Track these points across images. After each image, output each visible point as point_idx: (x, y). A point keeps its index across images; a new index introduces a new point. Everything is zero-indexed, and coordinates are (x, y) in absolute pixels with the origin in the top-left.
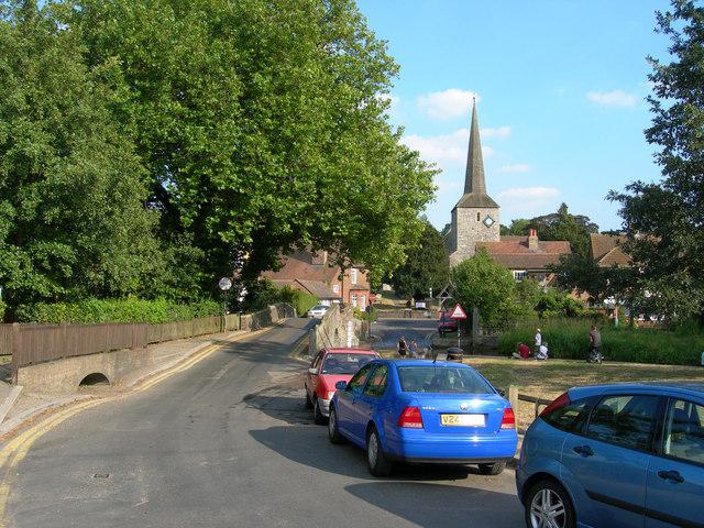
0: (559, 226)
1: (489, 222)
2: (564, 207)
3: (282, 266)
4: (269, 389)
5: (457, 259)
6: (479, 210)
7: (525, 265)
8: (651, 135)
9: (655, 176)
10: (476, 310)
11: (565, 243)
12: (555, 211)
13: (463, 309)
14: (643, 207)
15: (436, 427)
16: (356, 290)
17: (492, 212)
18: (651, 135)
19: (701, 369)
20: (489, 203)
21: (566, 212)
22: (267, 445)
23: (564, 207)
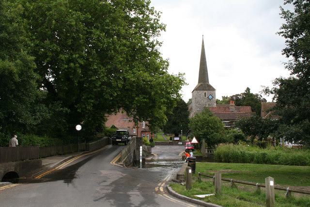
0: (248, 100)
1: (210, 97)
2: (248, 89)
3: (276, 83)
4: (280, 189)
5: (192, 116)
6: (205, 92)
7: (230, 118)
8: (287, 52)
9: (287, 74)
10: (204, 141)
11: (245, 107)
12: (243, 91)
13: (196, 138)
14: (286, 88)
15: (47, 169)
16: (144, 132)
17: (210, 92)
18: (287, 52)
19: (307, 167)
20: (211, 89)
21: (249, 91)
22: (47, 181)
23: (248, 89)
